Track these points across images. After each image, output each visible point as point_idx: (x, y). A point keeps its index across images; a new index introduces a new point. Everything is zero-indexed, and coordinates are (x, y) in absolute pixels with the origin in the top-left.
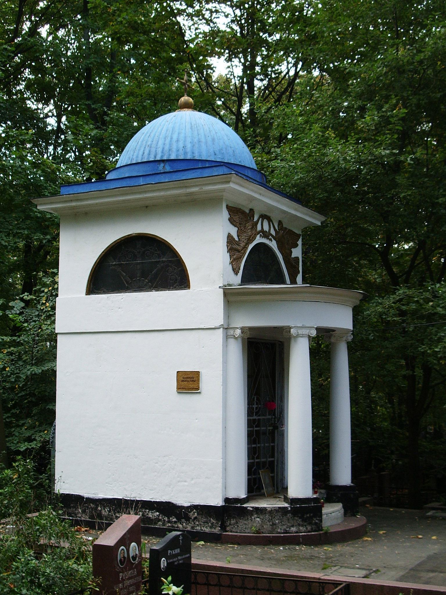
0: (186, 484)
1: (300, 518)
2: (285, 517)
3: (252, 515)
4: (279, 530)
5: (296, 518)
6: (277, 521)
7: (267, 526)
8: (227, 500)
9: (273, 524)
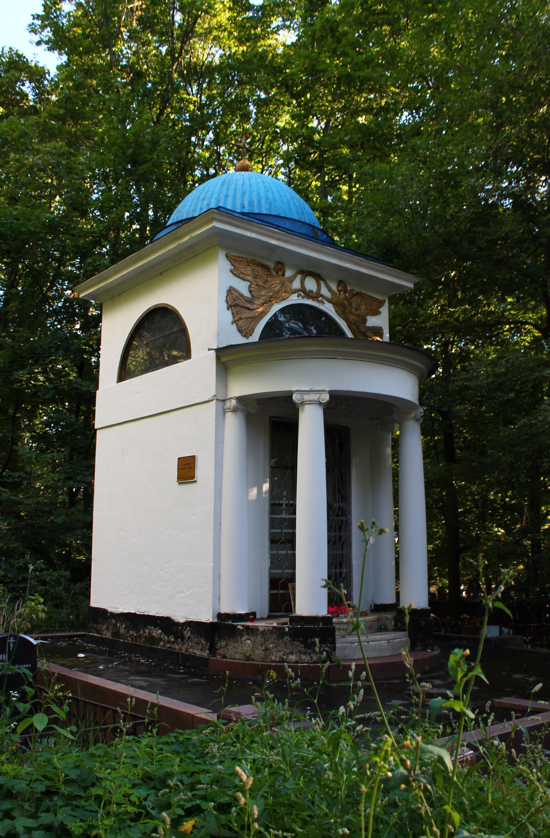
0: (183, 595)
1: (302, 643)
2: (280, 641)
3: (242, 636)
4: (273, 658)
5: (296, 643)
6: (271, 646)
7: (259, 653)
8: (220, 616)
9: (267, 649)
